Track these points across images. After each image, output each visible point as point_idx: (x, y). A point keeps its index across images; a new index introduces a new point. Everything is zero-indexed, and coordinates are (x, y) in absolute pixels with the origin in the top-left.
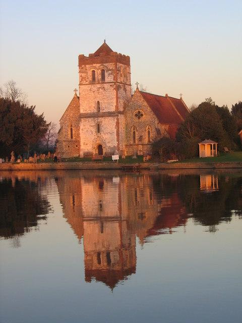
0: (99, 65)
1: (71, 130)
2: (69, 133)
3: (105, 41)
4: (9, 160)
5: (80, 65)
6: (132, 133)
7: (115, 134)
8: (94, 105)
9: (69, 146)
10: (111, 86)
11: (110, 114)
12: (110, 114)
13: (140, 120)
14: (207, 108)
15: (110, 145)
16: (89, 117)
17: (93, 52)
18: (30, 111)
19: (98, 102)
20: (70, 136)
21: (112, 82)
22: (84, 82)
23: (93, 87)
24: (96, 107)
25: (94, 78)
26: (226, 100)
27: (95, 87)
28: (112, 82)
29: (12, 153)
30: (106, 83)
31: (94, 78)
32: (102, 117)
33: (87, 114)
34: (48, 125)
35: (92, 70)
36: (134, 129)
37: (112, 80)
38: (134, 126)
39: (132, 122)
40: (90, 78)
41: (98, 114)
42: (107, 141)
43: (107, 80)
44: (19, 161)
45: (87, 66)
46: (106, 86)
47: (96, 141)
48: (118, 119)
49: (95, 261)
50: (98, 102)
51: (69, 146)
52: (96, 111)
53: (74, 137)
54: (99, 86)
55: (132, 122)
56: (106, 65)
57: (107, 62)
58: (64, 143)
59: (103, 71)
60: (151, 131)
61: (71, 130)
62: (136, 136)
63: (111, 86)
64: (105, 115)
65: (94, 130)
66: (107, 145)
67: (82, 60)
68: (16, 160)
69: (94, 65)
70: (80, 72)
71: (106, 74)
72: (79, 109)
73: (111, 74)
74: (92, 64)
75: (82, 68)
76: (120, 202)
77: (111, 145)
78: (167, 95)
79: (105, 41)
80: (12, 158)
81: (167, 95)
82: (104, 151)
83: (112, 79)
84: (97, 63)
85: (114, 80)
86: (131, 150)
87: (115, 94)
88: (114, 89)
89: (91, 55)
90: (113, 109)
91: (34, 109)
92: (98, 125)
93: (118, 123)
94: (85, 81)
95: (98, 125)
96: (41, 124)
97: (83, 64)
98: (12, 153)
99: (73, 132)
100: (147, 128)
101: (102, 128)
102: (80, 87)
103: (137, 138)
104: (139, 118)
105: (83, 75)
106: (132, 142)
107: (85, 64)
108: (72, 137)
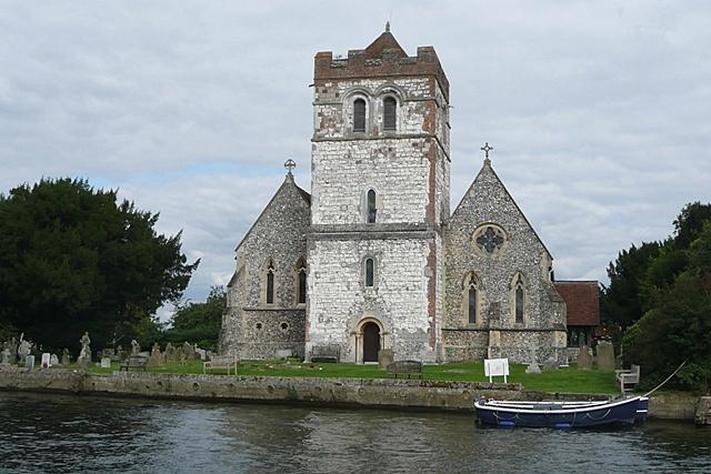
0: (379, 83)
1: (270, 276)
2: (264, 286)
3: (388, 25)
4: (74, 359)
5: (318, 81)
6: (465, 293)
7: (425, 291)
8: (357, 201)
9: (259, 326)
10: (415, 145)
11: (409, 232)
12: (409, 232)
13: (494, 256)
15: (405, 325)
16: (344, 238)
17: (362, 45)
18: (143, 223)
19: (372, 193)
20: (264, 295)
21: (419, 136)
22: (329, 132)
24: (365, 207)
25: (360, 123)
26: (704, 203)
27: (361, 150)
28: (419, 136)
29: (86, 340)
31: (360, 123)
32: (384, 238)
33: (333, 229)
34: (189, 268)
35: (356, 97)
36: (473, 280)
37: (419, 130)
38: (473, 272)
40: (349, 122)
41: (372, 230)
42: (396, 313)
43: (401, 128)
44: (105, 363)
45: (342, 85)
46: (396, 144)
47: (361, 311)
48: (433, 247)
50: (372, 193)
51: (259, 326)
52: (362, 219)
53: (276, 300)
54: (374, 145)
56: (400, 83)
58: (245, 315)
59: (390, 102)
61: (270, 276)
62: (480, 302)
63: (415, 145)
64: (393, 233)
65: (356, 277)
67: (327, 69)
68: (96, 358)
69: (363, 83)
70: (317, 102)
71: (400, 111)
72: (310, 214)
73: (417, 111)
75: (325, 92)
77: (409, 326)
79: (388, 25)
80: (83, 353)
82: (386, 343)
83: (419, 127)
85: (425, 127)
86: (460, 345)
87: (428, 170)
88: (426, 155)
89: (355, 56)
90: (417, 215)
91: (153, 221)
92: (370, 262)
93: (432, 260)
94: (331, 130)
95: (370, 262)
96: (169, 266)
97: (327, 80)
98: (86, 340)
99: (276, 285)
100: (514, 282)
101: (381, 274)
102: (314, 148)
103: (479, 309)
105: (327, 111)
106: (465, 322)
107: (336, 80)
108: (270, 300)
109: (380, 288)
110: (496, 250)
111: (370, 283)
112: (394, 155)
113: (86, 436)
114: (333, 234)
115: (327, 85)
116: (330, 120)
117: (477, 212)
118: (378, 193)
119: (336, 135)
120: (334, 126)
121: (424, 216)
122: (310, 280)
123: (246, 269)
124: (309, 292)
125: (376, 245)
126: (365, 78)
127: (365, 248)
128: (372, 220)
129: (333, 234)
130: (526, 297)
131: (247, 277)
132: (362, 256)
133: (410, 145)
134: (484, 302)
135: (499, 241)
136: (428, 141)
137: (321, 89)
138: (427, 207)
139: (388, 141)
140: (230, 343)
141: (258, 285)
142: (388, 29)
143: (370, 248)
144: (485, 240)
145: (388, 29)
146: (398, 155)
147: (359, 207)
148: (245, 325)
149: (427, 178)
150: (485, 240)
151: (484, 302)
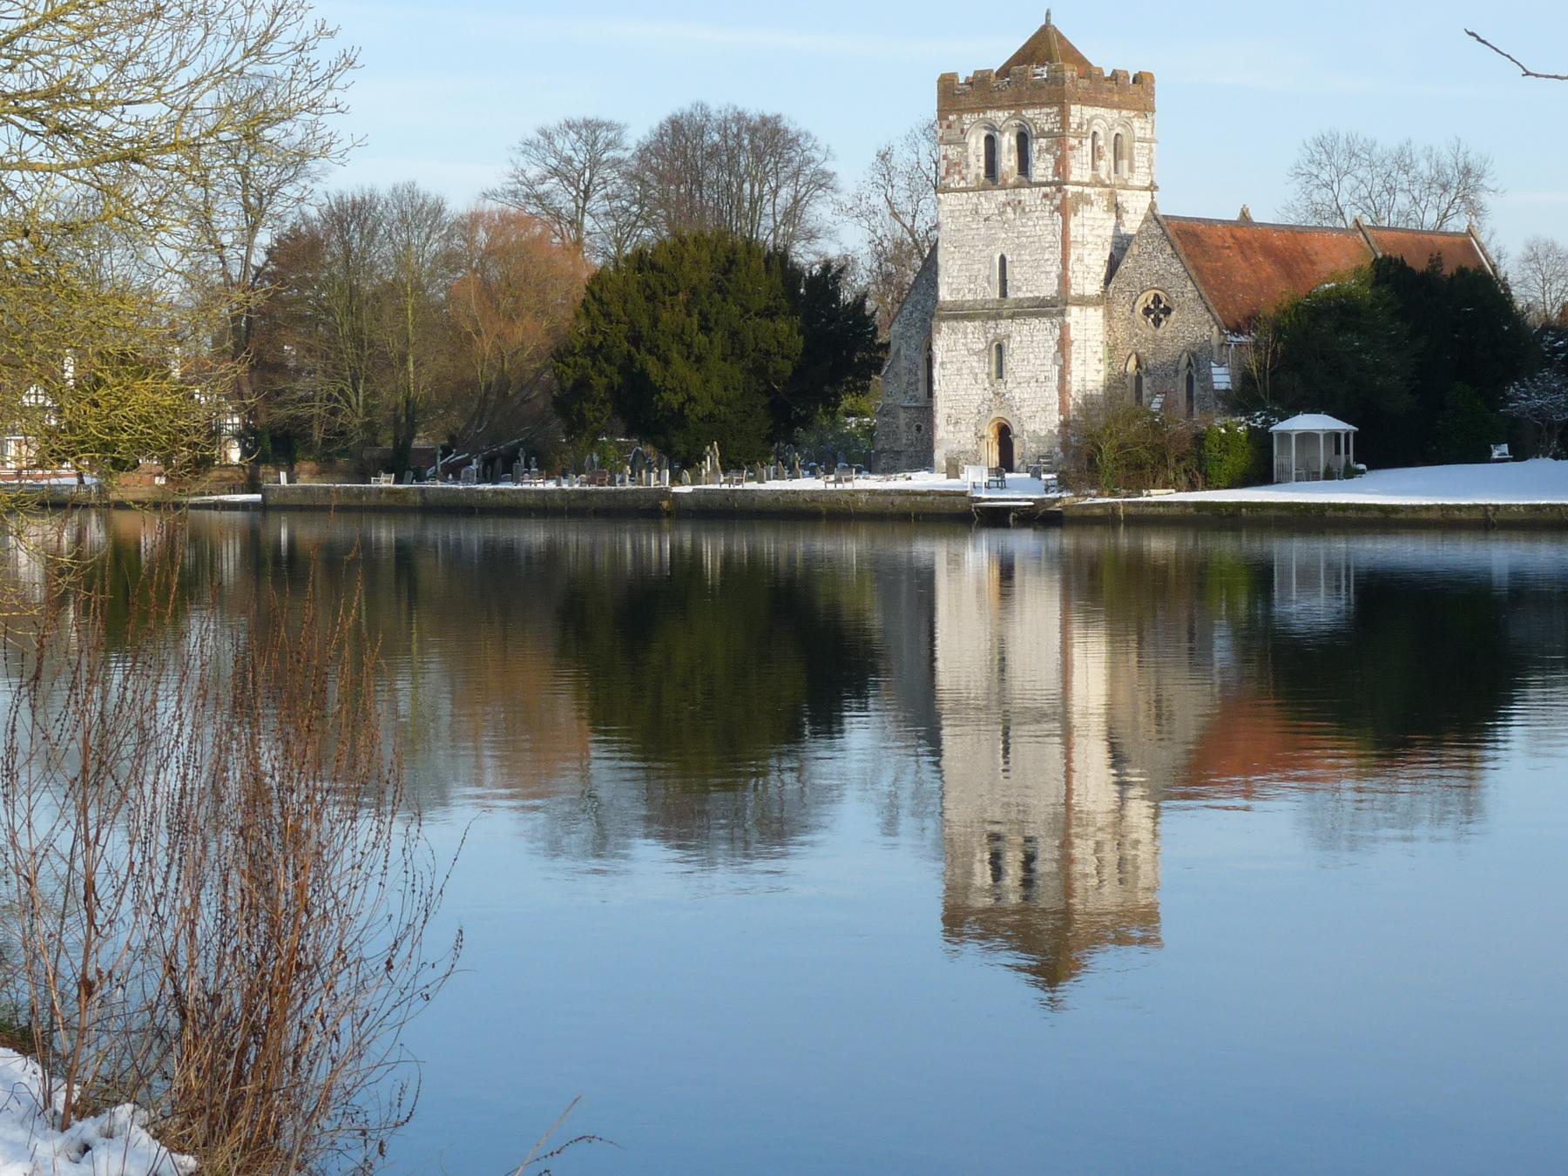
2: (921, 374)
3: (1048, 14)
5: (943, 113)
7: (1055, 383)
9: (919, 428)
13: (1160, 332)
14: (1411, 268)
19: (1003, 259)
23: (983, 199)
30: (1031, 185)
32: (1012, 317)
39: (1131, 339)
40: (977, 166)
42: (1026, 411)
47: (990, 410)
48: (1064, 328)
49: (982, 875)
50: (1003, 259)
51: (919, 428)
55: (1131, 339)
56: (1029, 113)
57: (1033, 105)
58: (902, 415)
59: (1023, 140)
60: (1195, 376)
63: (1045, 196)
65: (983, 367)
66: (1027, 427)
73: (1048, 150)
74: (983, 109)
75: (949, 127)
76: (1226, 808)
78: (1244, 214)
79: (1048, 14)
81: (1244, 214)
84: (999, 108)
85: (1056, 172)
87: (1059, 229)
88: (1057, 209)
92: (1000, 348)
101: (1010, 363)
104: (1157, 322)
107: (960, 112)
109: (1009, 380)
110: (1163, 323)
111: (1000, 374)
112: (1024, 209)
113: (1031, 503)
114: (961, 313)
115: (950, 117)
116: (955, 164)
117: (1141, 274)
118: (1008, 258)
119: (963, 184)
120: (960, 172)
121: (1056, 288)
122: (936, 373)
123: (902, 353)
124: (936, 387)
125: (1005, 326)
126: (991, 108)
127: (993, 331)
128: (1004, 294)
129: (961, 313)
130: (1196, 384)
131: (904, 363)
132: (989, 340)
133: (1041, 195)
134: (1149, 392)
135: (1167, 311)
136: (1059, 190)
137: (945, 123)
138: (1058, 277)
139: (1017, 190)
140: (883, 451)
141: (916, 375)
142: (1048, 21)
143: (998, 331)
144: (1162, 311)
145: (1048, 21)
146: (1027, 209)
147: (989, 277)
148: (903, 427)
149: (1059, 238)
150: (1162, 311)
151: (1149, 392)
